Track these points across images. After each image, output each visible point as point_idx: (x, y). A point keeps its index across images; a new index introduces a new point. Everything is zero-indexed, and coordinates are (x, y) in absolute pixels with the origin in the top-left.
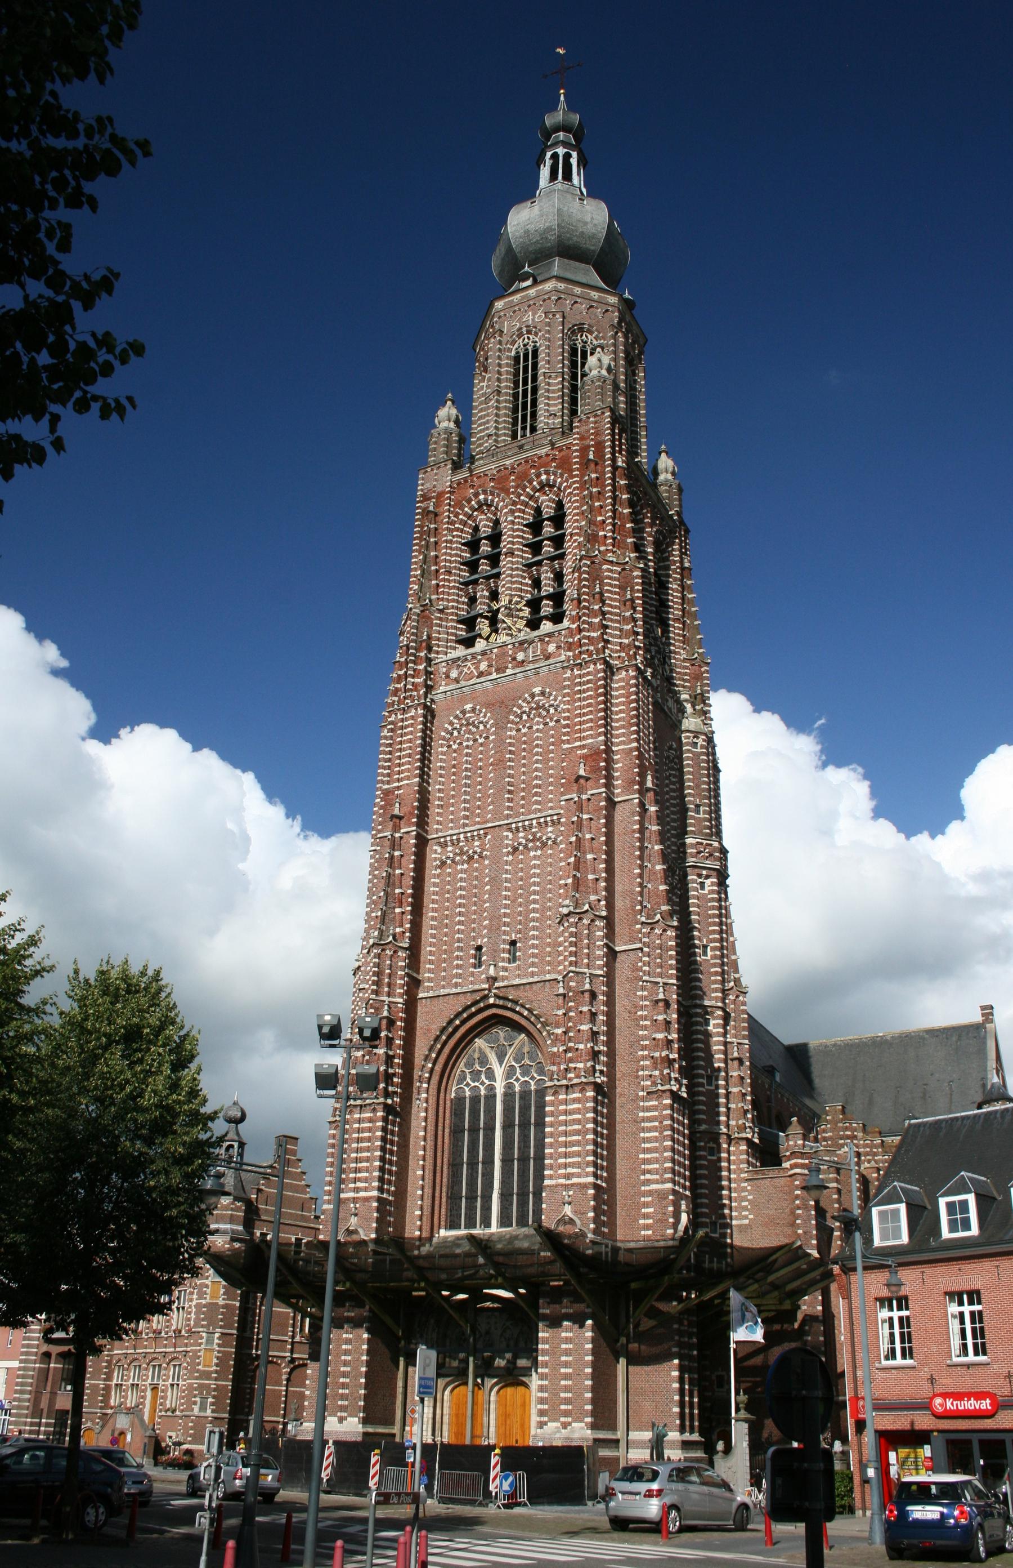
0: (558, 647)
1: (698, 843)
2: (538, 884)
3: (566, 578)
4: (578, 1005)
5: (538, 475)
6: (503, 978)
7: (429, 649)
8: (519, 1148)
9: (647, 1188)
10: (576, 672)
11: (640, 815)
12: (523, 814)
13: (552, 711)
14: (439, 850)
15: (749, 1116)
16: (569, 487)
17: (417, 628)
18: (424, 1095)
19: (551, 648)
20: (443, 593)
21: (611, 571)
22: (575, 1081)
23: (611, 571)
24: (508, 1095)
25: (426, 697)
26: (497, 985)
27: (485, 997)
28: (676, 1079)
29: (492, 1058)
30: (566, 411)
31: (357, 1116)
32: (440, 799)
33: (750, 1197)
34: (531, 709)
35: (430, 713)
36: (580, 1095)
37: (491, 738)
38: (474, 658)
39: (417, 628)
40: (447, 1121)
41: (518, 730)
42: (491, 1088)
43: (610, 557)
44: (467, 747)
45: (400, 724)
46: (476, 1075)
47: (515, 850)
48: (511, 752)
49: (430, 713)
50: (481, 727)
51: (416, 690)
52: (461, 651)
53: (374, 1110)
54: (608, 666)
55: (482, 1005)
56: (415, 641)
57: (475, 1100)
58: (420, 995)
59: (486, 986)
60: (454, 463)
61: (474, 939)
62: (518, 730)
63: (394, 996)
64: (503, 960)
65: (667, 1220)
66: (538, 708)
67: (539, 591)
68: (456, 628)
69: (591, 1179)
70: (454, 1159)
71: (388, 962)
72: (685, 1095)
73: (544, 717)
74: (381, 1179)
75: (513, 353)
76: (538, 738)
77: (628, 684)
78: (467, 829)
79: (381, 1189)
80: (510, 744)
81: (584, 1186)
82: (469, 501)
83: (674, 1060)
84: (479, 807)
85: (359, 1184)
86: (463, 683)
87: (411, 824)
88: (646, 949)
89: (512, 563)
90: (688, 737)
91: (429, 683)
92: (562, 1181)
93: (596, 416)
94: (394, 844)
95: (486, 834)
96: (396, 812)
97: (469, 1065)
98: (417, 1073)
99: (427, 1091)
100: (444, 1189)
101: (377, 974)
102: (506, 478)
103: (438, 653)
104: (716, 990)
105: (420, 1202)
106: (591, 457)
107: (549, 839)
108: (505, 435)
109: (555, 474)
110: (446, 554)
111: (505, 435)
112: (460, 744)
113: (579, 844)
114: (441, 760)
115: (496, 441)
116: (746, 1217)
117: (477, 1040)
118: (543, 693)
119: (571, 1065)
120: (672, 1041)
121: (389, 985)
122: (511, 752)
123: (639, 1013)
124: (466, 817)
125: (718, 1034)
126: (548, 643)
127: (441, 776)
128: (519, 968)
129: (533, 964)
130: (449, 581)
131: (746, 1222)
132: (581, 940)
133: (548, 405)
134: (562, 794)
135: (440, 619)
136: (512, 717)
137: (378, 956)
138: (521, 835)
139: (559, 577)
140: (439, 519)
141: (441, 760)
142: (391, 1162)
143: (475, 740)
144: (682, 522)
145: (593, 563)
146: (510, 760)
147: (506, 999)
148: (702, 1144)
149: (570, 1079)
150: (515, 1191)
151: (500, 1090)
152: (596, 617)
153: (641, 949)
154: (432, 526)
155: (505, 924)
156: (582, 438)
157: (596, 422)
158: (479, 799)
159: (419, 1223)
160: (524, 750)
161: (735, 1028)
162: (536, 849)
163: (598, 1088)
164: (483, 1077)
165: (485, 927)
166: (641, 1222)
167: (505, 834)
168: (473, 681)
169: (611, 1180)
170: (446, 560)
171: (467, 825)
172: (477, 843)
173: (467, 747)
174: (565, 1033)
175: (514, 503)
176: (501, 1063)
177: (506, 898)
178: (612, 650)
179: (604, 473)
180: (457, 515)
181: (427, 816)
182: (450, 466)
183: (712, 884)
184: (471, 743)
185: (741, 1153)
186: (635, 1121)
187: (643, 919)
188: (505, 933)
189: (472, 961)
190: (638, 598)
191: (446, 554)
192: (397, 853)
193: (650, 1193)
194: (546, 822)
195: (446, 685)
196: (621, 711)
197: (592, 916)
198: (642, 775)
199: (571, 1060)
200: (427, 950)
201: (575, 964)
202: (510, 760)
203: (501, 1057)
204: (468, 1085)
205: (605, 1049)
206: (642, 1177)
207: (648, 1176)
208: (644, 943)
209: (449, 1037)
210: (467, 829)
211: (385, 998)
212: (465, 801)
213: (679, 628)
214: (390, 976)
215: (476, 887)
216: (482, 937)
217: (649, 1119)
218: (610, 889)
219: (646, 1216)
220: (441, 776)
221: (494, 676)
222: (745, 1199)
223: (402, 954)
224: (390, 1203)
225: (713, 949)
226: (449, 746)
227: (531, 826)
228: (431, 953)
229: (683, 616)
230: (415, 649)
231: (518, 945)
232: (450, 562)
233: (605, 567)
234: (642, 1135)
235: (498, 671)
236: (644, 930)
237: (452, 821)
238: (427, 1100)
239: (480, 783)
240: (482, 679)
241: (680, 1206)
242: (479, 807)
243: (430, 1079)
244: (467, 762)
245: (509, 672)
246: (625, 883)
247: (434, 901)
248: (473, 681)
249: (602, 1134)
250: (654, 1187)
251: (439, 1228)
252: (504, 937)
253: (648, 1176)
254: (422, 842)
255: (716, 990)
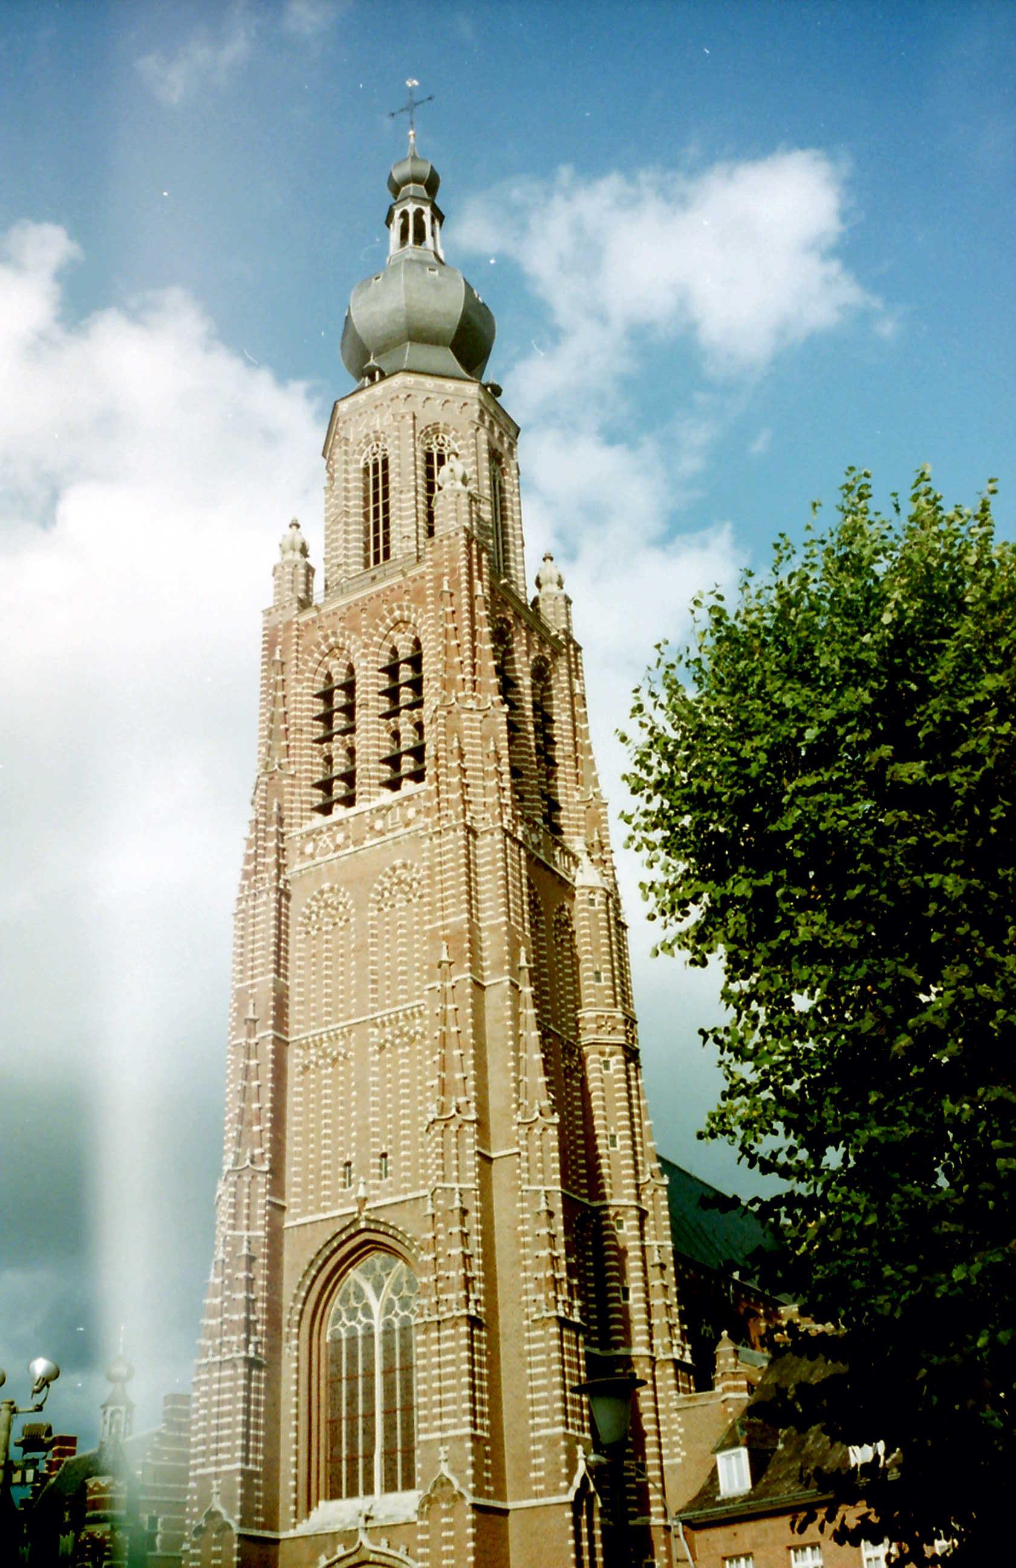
0: (418, 812)
1: (598, 1017)
2: (407, 1086)
3: (426, 730)
4: (447, 1226)
5: (391, 612)
6: (375, 1198)
7: (281, 821)
8: (402, 1396)
9: (537, 1434)
10: (436, 841)
11: (512, 999)
12: (389, 1006)
13: (415, 885)
14: (301, 1052)
15: (677, 1331)
16: (424, 623)
17: (266, 799)
18: (294, 1342)
19: (411, 813)
20: (294, 755)
21: (472, 720)
22: (448, 1315)
23: (472, 720)
24: (388, 1331)
25: (278, 878)
26: (368, 1206)
27: (355, 1221)
28: (564, 1302)
29: (368, 1289)
30: (421, 531)
31: (216, 1374)
32: (300, 994)
33: (681, 1430)
34: (393, 884)
35: (283, 894)
36: (452, 1331)
37: (352, 920)
38: (329, 829)
39: (266, 799)
40: (323, 1371)
41: (380, 910)
42: (369, 1328)
43: (471, 704)
44: (327, 932)
45: (251, 912)
46: (352, 1314)
47: (382, 1047)
48: (372, 936)
49: (283, 894)
50: (341, 908)
51: (267, 871)
52: (319, 820)
53: (235, 1366)
54: (470, 830)
55: (352, 1230)
56: (265, 815)
57: (352, 1340)
58: (286, 1225)
59: (356, 1209)
60: (300, 601)
61: (342, 1154)
62: (380, 910)
63: (256, 1228)
64: (373, 1176)
65: (559, 1471)
66: (400, 882)
67: (399, 745)
68: (311, 795)
69: (469, 1430)
70: (332, 1414)
71: (246, 1190)
72: (577, 1319)
73: (406, 893)
74: (246, 1448)
75: (362, 465)
76: (401, 918)
77: (493, 849)
78: (331, 1027)
79: (246, 1460)
80: (372, 927)
81: (460, 1439)
82: (318, 645)
83: (562, 1279)
84: (342, 1001)
85: (221, 1456)
86: (318, 859)
87: (267, 1027)
88: (524, 1154)
89: (367, 715)
90: (583, 894)
91: (282, 861)
92: (438, 1435)
93: (449, 538)
94: (249, 1051)
95: (350, 1032)
96: (251, 1016)
97: (345, 1300)
98: (286, 1317)
99: (298, 1336)
100: (322, 1451)
101: (234, 1206)
102: (355, 616)
103: (291, 825)
104: (627, 1187)
105: (294, 1471)
106: (446, 588)
107: (416, 1033)
108: (356, 563)
109: (408, 608)
110: (295, 709)
111: (356, 563)
112: (319, 929)
113: (443, 1040)
114: (300, 950)
115: (346, 571)
116: (678, 1455)
117: (350, 1270)
118: (404, 866)
119: (443, 1297)
120: (558, 1258)
121: (248, 1217)
122: (372, 936)
123: (520, 1228)
124: (328, 1014)
125: (633, 1238)
126: (408, 807)
127: (300, 967)
128: (391, 1184)
129: (405, 1180)
130: (301, 740)
131: (678, 1460)
132: (449, 1150)
133: (400, 525)
134: (425, 982)
135: (292, 786)
136: (372, 895)
137: (235, 1184)
138: (388, 1030)
139: (419, 727)
140: (286, 667)
141: (300, 950)
142: (257, 1427)
143: (335, 924)
144: (570, 640)
145: (449, 712)
146: (373, 945)
147: (377, 1222)
148: (621, 1371)
149: (442, 1313)
150: (399, 1447)
151: (378, 1330)
152: (454, 776)
153: (519, 1154)
154: (280, 678)
155: (374, 1135)
156: (436, 565)
157: (450, 546)
158: (342, 992)
159: (293, 1496)
160: (387, 932)
161: (655, 1228)
162: (404, 1045)
163: (473, 1322)
164: (360, 1315)
165: (353, 1140)
166: (533, 1475)
167: (370, 1030)
168: (330, 856)
169: (496, 1428)
170: (295, 717)
171: (330, 1022)
172: (341, 1043)
173: (327, 932)
174: (435, 1259)
175: (366, 646)
176: (378, 1296)
177: (374, 1104)
178: (476, 812)
179: (460, 605)
180: (305, 663)
181: (287, 1015)
182: (296, 605)
183: (618, 1062)
184: (331, 927)
185: (668, 1377)
186: (521, 1355)
187: (520, 1119)
188: (374, 1145)
189: (341, 1180)
190: (503, 748)
191: (295, 709)
192: (253, 1062)
193: (540, 1439)
194: (413, 1014)
195: (302, 862)
196: (487, 882)
197: (460, 1122)
198: (514, 955)
199: (442, 1291)
200: (292, 1173)
201: (444, 1178)
202: (373, 945)
203: (378, 1288)
204: (344, 1325)
205: (482, 1274)
206: (531, 1422)
207: (538, 1420)
208: (522, 1147)
209: (319, 1271)
210: (331, 1027)
211: (245, 1233)
212: (327, 995)
213: (570, 766)
214: (249, 1206)
215: (342, 1093)
216: (350, 1150)
217: (536, 1352)
218: (482, 1087)
219: (537, 1468)
220: (300, 967)
221: (352, 849)
222: (675, 1433)
223: (261, 1179)
224: (256, 1475)
225: (622, 1138)
226: (308, 933)
227: (397, 1019)
228: (296, 1174)
229: (576, 751)
230: (265, 823)
231: (389, 1157)
232: (301, 718)
233: (464, 716)
234: (528, 1371)
235: (355, 843)
236: (521, 1132)
237: (314, 1019)
238: (298, 1349)
239: (342, 973)
240: (339, 853)
241: (576, 1452)
242: (342, 1001)
243: (300, 1322)
244: (327, 950)
245: (367, 843)
246: (499, 1081)
247: (297, 1114)
248: (330, 856)
249: (481, 1375)
250: (544, 1432)
251: (318, 1499)
252: (374, 1150)
253: (538, 1420)
254: (281, 1045)
255: (627, 1187)
